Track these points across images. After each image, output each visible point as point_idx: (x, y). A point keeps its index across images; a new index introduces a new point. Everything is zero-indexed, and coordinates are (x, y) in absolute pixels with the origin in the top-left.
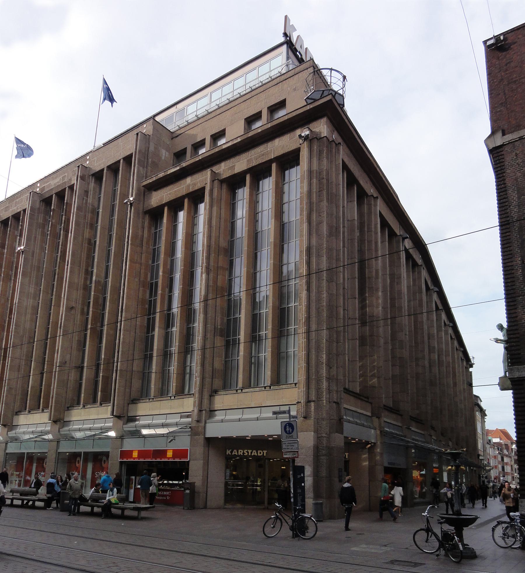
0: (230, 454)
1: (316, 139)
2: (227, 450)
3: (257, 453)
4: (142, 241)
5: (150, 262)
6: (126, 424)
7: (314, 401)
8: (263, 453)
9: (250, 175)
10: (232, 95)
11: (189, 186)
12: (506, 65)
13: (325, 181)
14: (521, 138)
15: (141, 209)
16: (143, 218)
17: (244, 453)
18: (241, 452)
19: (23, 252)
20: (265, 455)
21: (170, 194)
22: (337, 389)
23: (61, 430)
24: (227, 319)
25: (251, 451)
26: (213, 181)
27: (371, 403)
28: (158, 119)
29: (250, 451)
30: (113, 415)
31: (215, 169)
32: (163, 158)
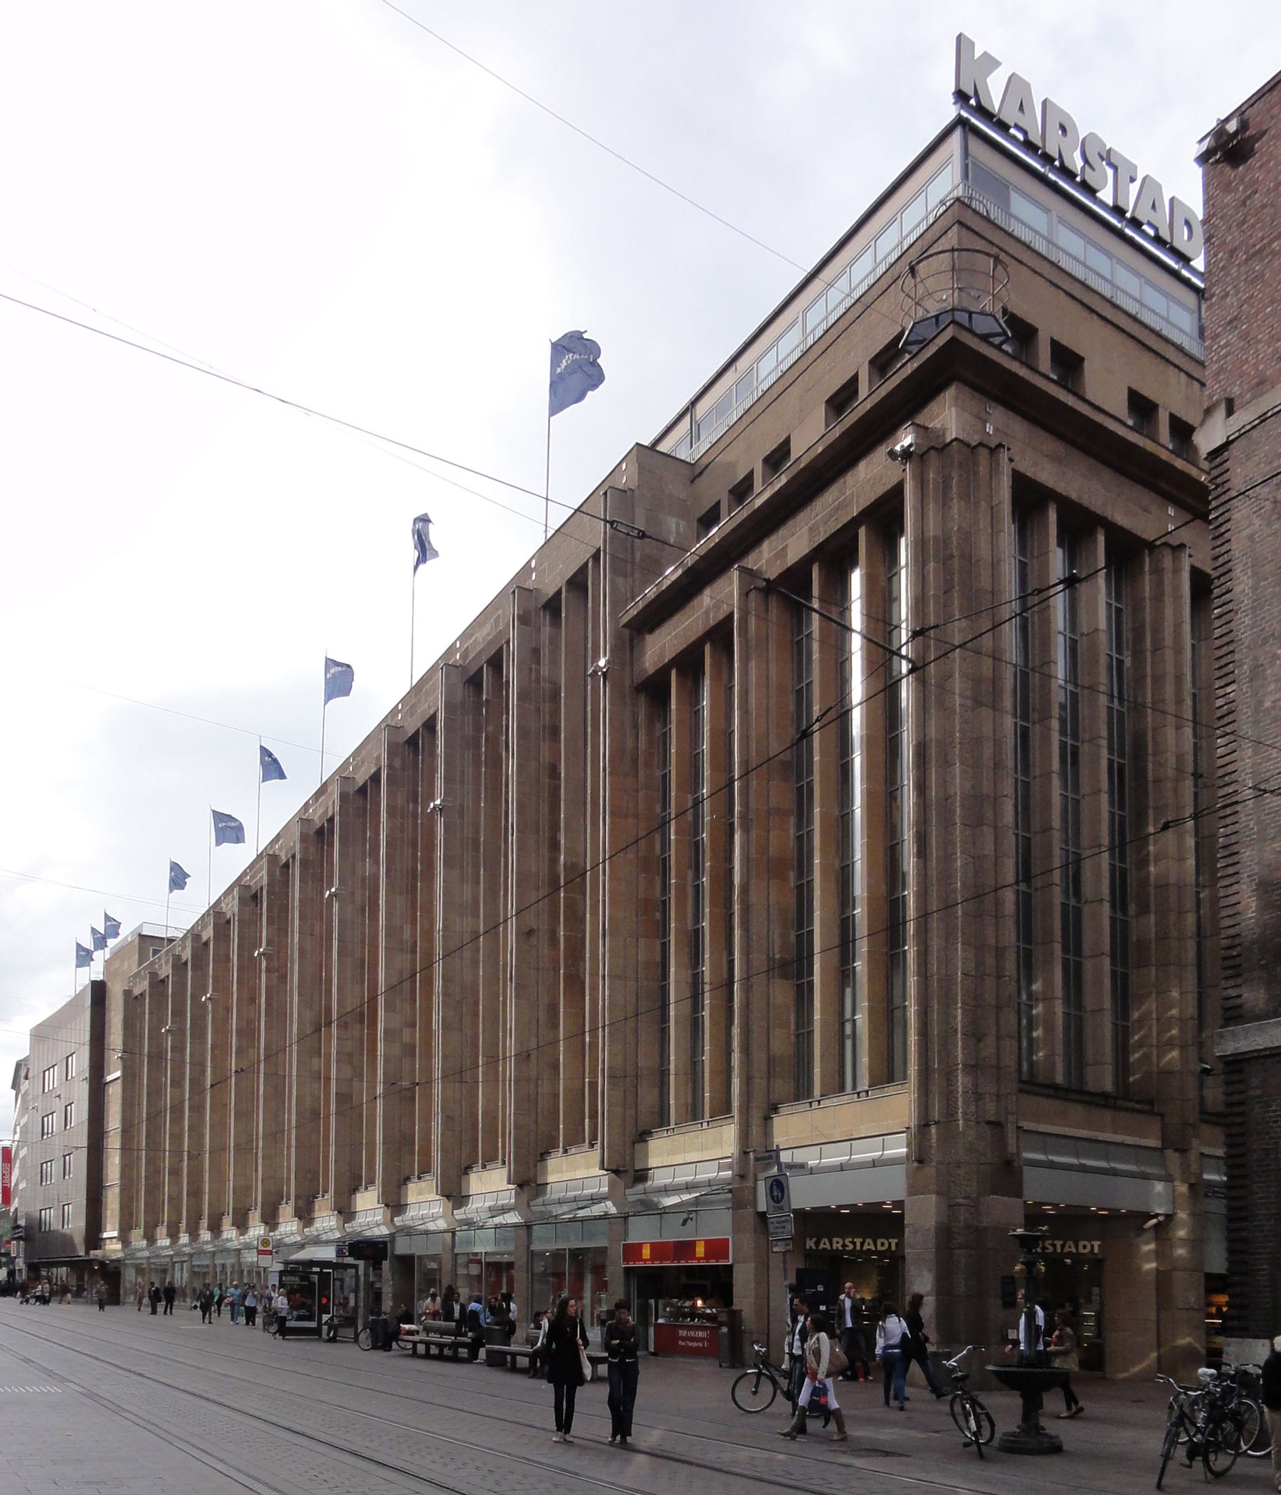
0: (814, 1248)
1: (932, 452)
3: (1077, 1248)
4: (635, 761)
5: (658, 808)
6: (632, 1187)
7: (936, 1123)
8: (890, 1244)
11: (707, 612)
13: (956, 563)
14: (1263, 419)
15: (627, 683)
17: (844, 1245)
18: (837, 1244)
19: (440, 809)
20: (893, 1248)
21: (676, 637)
22: (998, 1089)
23: (531, 1203)
25: (1061, 1242)
26: (747, 594)
27: (1162, 1115)
29: (858, 1241)
30: (602, 1168)
31: (751, 561)
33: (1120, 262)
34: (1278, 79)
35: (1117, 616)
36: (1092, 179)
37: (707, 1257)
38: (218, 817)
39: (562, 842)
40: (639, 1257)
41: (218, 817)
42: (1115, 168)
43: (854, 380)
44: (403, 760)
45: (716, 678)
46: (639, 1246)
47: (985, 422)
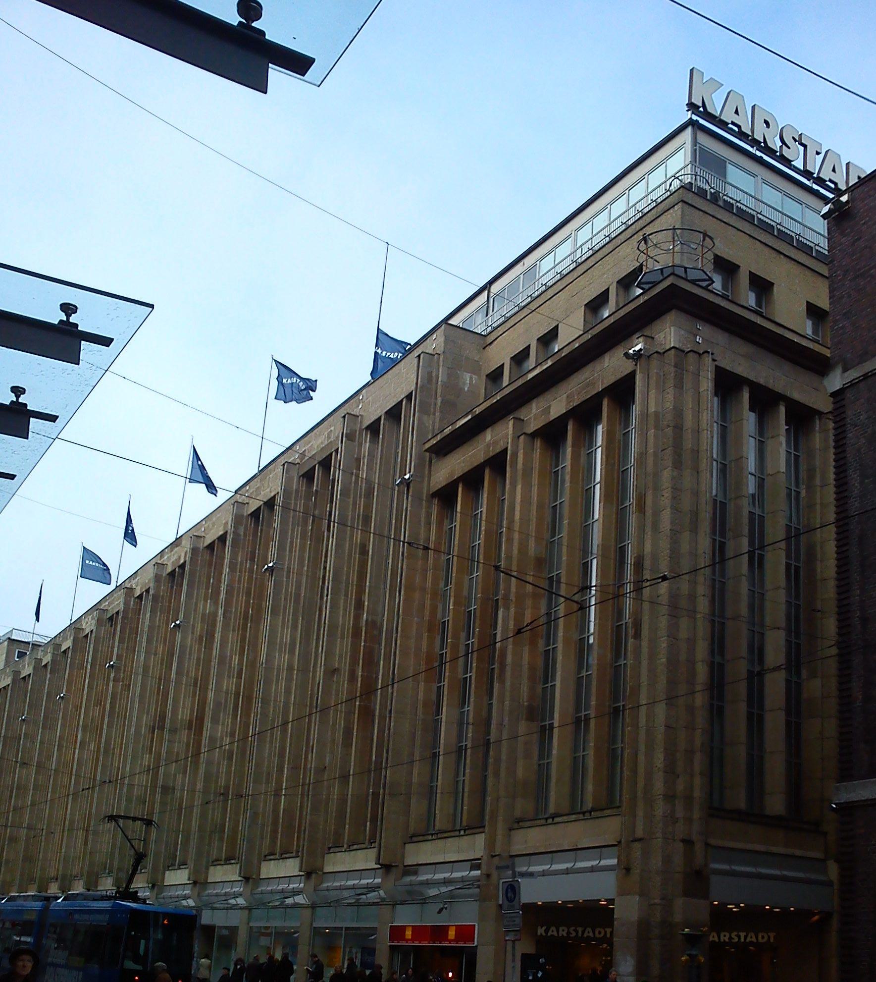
0: (544, 934)
2: (539, 927)
8: (769, 937)
9: (463, 484)
10: (664, 189)
11: (488, 446)
12: (853, 244)
14: (866, 376)
16: (429, 507)
17: (731, 938)
20: (772, 940)
24: (543, 688)
28: (453, 321)
32: (466, 389)
33: (808, 206)
34: (873, 175)
35: (794, 462)
36: (786, 152)
37: (457, 940)
38: (87, 553)
39: (366, 603)
40: (403, 938)
41: (87, 553)
42: (805, 146)
43: (607, 292)
44: (246, 529)
45: (492, 493)
46: (403, 929)
47: (695, 336)
